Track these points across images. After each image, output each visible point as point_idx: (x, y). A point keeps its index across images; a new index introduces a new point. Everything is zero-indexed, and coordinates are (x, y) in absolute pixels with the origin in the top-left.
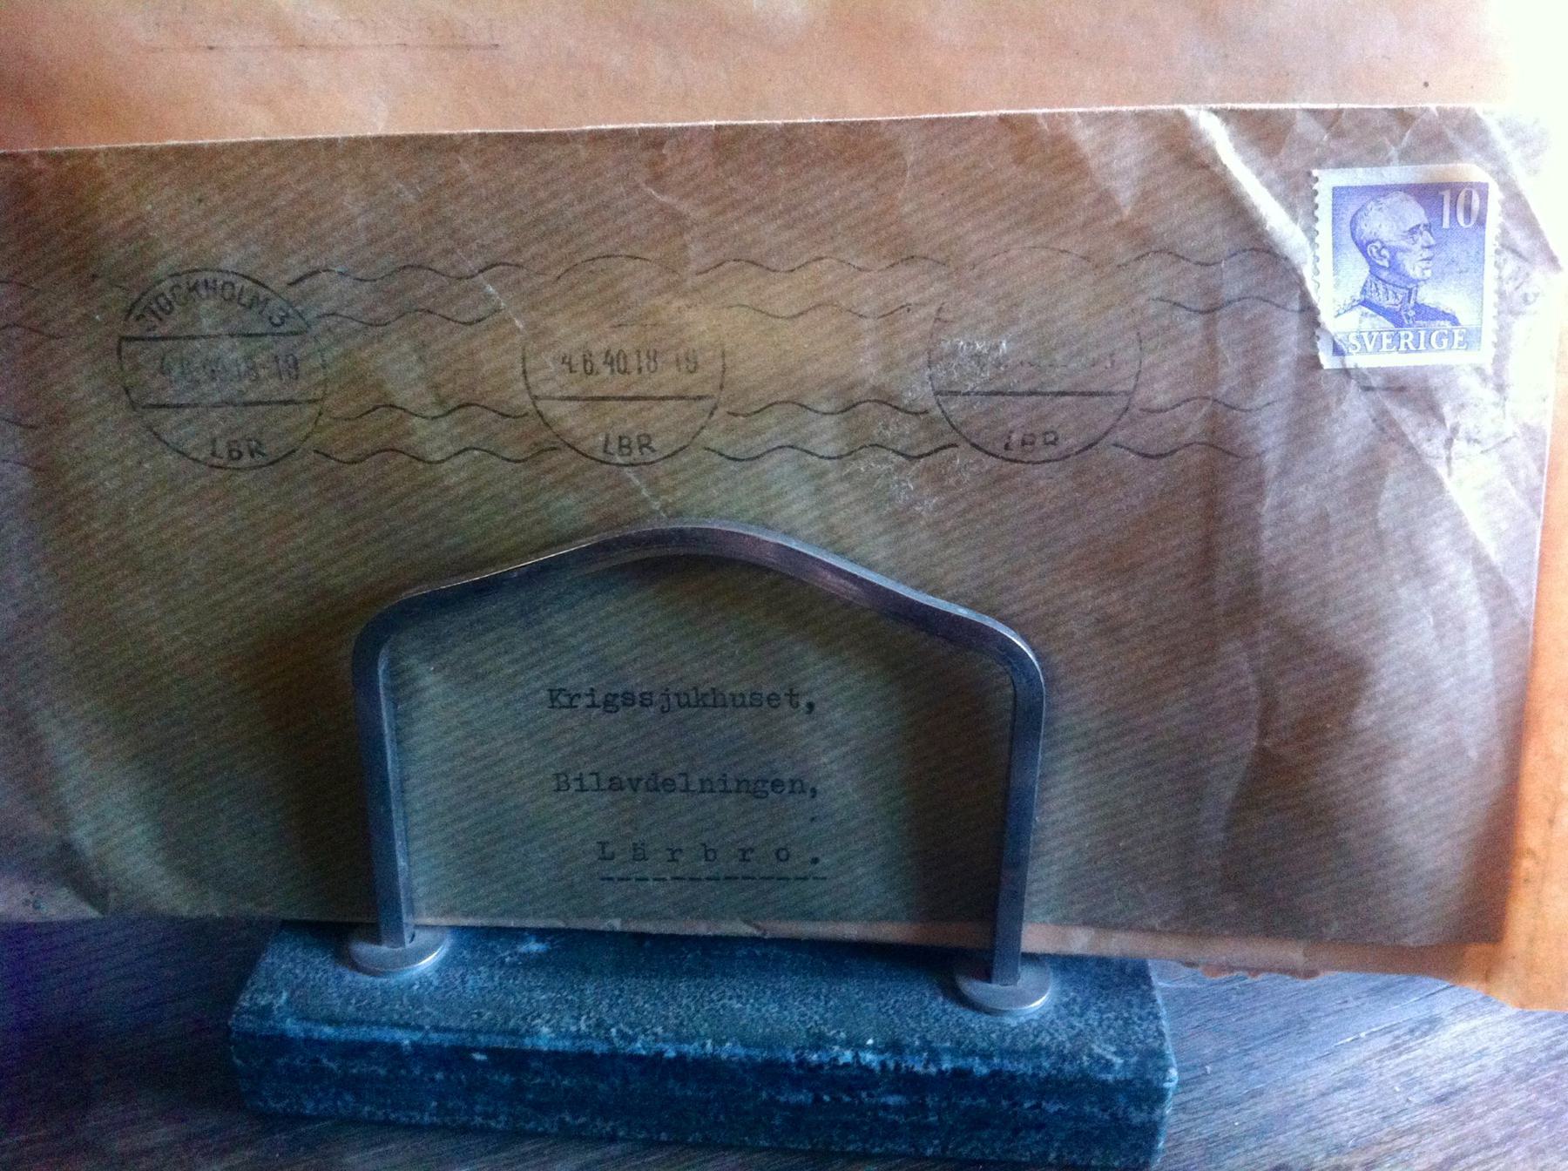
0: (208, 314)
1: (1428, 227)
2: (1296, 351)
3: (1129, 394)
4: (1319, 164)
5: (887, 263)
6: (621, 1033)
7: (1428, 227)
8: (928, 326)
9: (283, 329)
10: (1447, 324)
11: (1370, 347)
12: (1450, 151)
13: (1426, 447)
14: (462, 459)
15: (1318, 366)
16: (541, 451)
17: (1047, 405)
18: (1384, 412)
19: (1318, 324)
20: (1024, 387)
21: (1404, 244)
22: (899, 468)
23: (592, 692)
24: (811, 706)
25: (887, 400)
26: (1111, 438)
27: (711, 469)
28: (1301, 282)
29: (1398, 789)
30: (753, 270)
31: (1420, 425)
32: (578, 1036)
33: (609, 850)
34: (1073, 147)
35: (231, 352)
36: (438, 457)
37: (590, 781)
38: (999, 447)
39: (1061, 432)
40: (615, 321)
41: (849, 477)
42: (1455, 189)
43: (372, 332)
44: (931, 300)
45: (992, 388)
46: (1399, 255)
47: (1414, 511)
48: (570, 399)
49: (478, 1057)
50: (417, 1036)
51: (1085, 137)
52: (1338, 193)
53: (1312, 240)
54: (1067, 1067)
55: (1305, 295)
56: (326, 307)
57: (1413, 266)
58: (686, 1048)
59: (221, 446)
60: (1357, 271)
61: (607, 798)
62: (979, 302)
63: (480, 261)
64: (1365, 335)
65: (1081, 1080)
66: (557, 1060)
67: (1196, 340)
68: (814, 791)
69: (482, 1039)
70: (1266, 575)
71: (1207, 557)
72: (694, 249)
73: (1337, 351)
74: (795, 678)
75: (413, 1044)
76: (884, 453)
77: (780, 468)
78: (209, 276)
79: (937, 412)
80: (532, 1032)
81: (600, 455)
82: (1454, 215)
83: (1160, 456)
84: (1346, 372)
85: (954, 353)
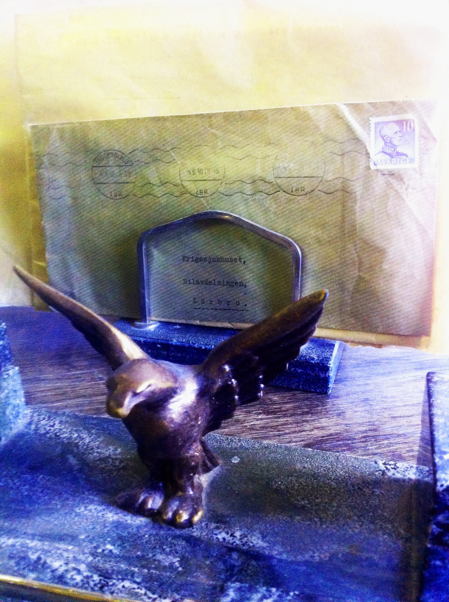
0: (111, 161)
1: (400, 131)
2: (365, 165)
3: (322, 177)
4: (371, 116)
5: (264, 145)
6: (192, 343)
7: (400, 131)
8: (273, 161)
9: (127, 164)
10: (405, 157)
11: (384, 163)
12: (405, 112)
13: (400, 190)
14: (165, 196)
15: (370, 169)
16: (182, 194)
17: (302, 180)
18: (388, 181)
19: (369, 158)
20: (296, 176)
21: (394, 136)
22: (266, 198)
23: (193, 257)
24: (244, 262)
25: (263, 180)
26: (318, 189)
27: (222, 198)
28: (365, 147)
29: (396, 287)
30: (232, 148)
31: (398, 185)
32: (182, 342)
33: (196, 301)
34: (309, 114)
35: (116, 170)
36: (160, 196)
37: (192, 281)
38: (290, 192)
39: (305, 187)
40: (201, 161)
41: (254, 200)
42: (407, 121)
43: (147, 165)
44: (274, 154)
45: (288, 176)
46: (392, 139)
47: (398, 208)
48: (189, 181)
49: (159, 346)
50: (145, 339)
51: (311, 112)
52: (377, 124)
53: (369, 136)
54: (302, 358)
55: (366, 150)
56: (137, 159)
57: (396, 142)
58: (207, 347)
59: (113, 194)
60: (381, 143)
61: (195, 286)
62: (286, 154)
63: (171, 147)
64: (383, 161)
65: (306, 362)
66: (176, 346)
67: (339, 162)
68: (245, 286)
69: (160, 341)
70: (358, 226)
71: (343, 221)
72: (219, 143)
73: (375, 164)
74: (240, 254)
75: (144, 341)
76: (262, 193)
77: (237, 198)
78: (111, 151)
79: (275, 182)
80: (172, 341)
81: (195, 195)
82: (406, 129)
83: (331, 193)
84: (377, 170)
85: (279, 167)
